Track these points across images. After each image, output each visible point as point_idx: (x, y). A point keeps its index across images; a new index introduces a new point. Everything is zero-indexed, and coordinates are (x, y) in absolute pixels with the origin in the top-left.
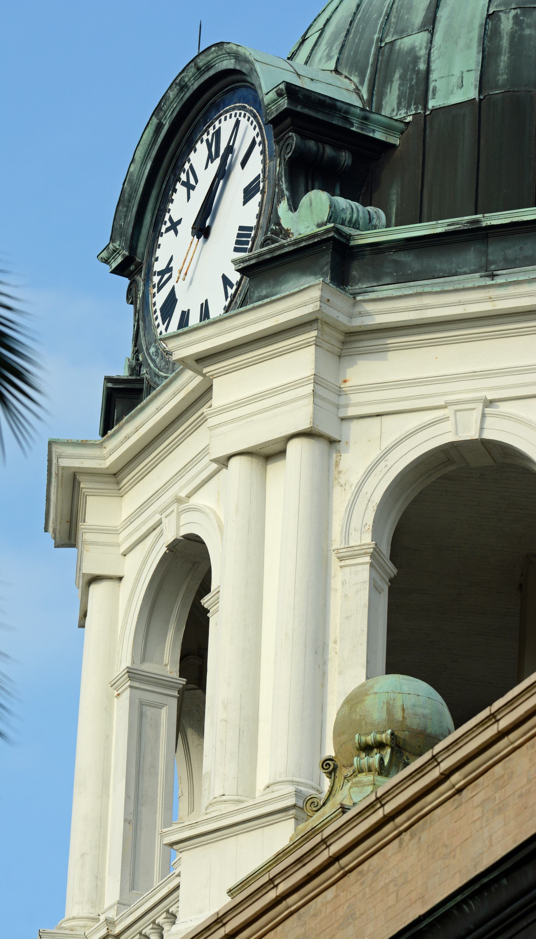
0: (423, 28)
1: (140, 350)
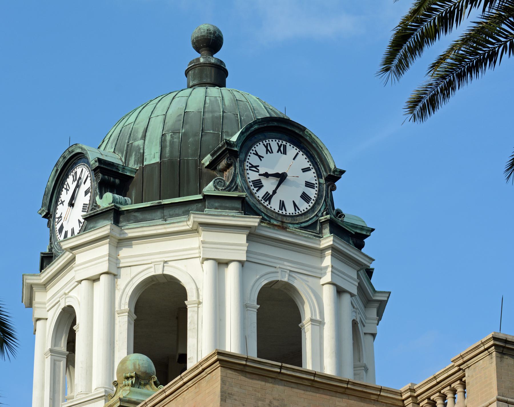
0: (141, 139)
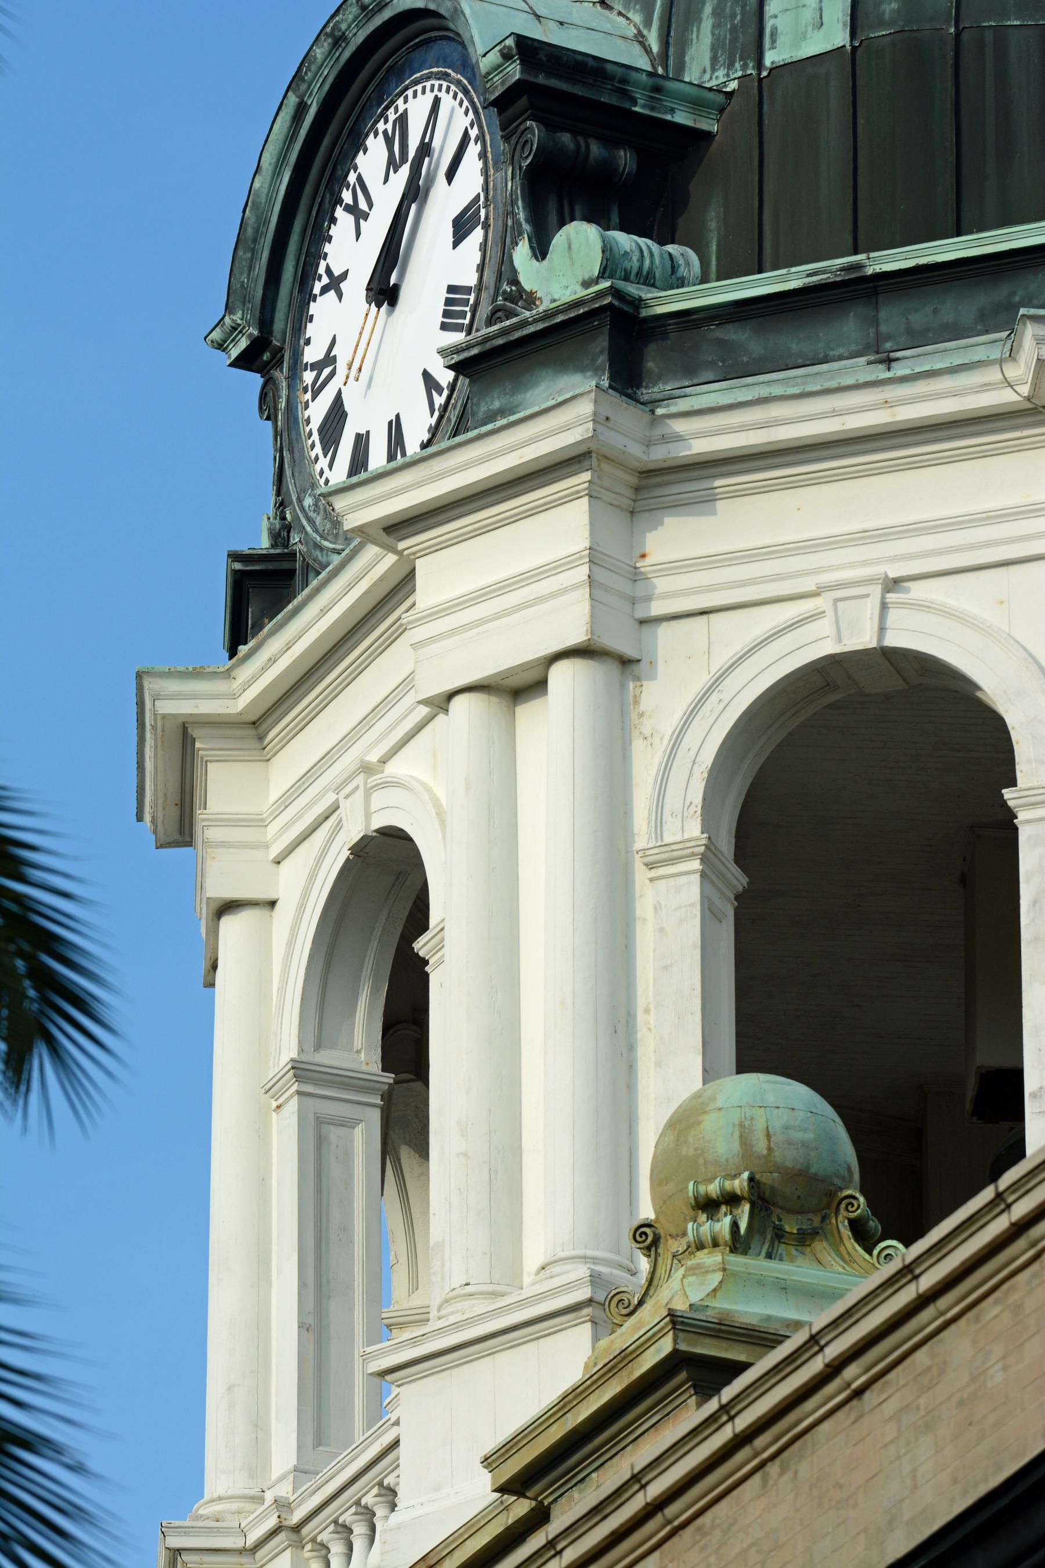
1: (286, 502)
